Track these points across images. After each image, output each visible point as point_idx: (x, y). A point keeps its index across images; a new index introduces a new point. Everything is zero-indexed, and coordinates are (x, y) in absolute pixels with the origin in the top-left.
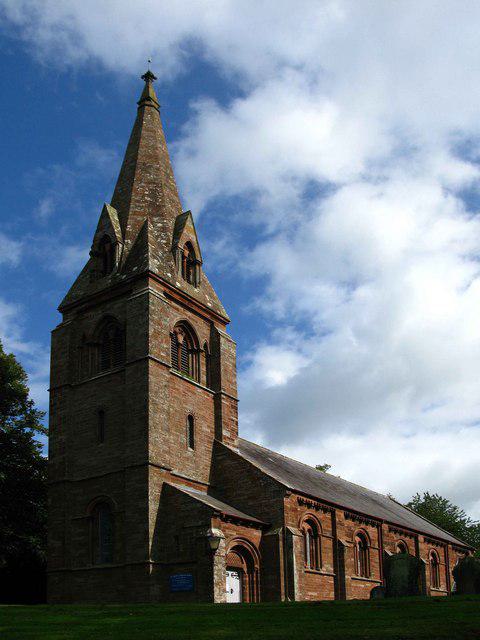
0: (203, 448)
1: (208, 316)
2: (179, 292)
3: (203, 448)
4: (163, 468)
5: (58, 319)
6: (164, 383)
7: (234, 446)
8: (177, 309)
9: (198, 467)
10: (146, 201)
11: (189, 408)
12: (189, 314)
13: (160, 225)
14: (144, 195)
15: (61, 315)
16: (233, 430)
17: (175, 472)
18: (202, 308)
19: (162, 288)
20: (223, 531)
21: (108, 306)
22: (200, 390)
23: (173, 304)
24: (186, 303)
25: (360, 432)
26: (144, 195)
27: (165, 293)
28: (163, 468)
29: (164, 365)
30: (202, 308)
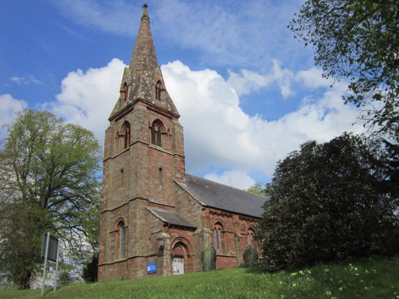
0: (167, 185)
1: (169, 115)
2: (154, 106)
3: (167, 185)
4: (145, 199)
5: (108, 124)
6: (146, 153)
7: (183, 182)
8: (154, 114)
9: (164, 197)
10: (142, 64)
11: (160, 165)
12: (160, 116)
13: (147, 74)
14: (141, 61)
15: (109, 122)
16: (182, 173)
17: (152, 201)
18: (165, 112)
19: (146, 105)
20: (170, 234)
21: (126, 117)
22: (165, 154)
23: (152, 112)
24: (158, 110)
25: (309, 146)
26: (141, 61)
27: (147, 108)
28: (145, 199)
29: (146, 144)
30: (165, 112)
